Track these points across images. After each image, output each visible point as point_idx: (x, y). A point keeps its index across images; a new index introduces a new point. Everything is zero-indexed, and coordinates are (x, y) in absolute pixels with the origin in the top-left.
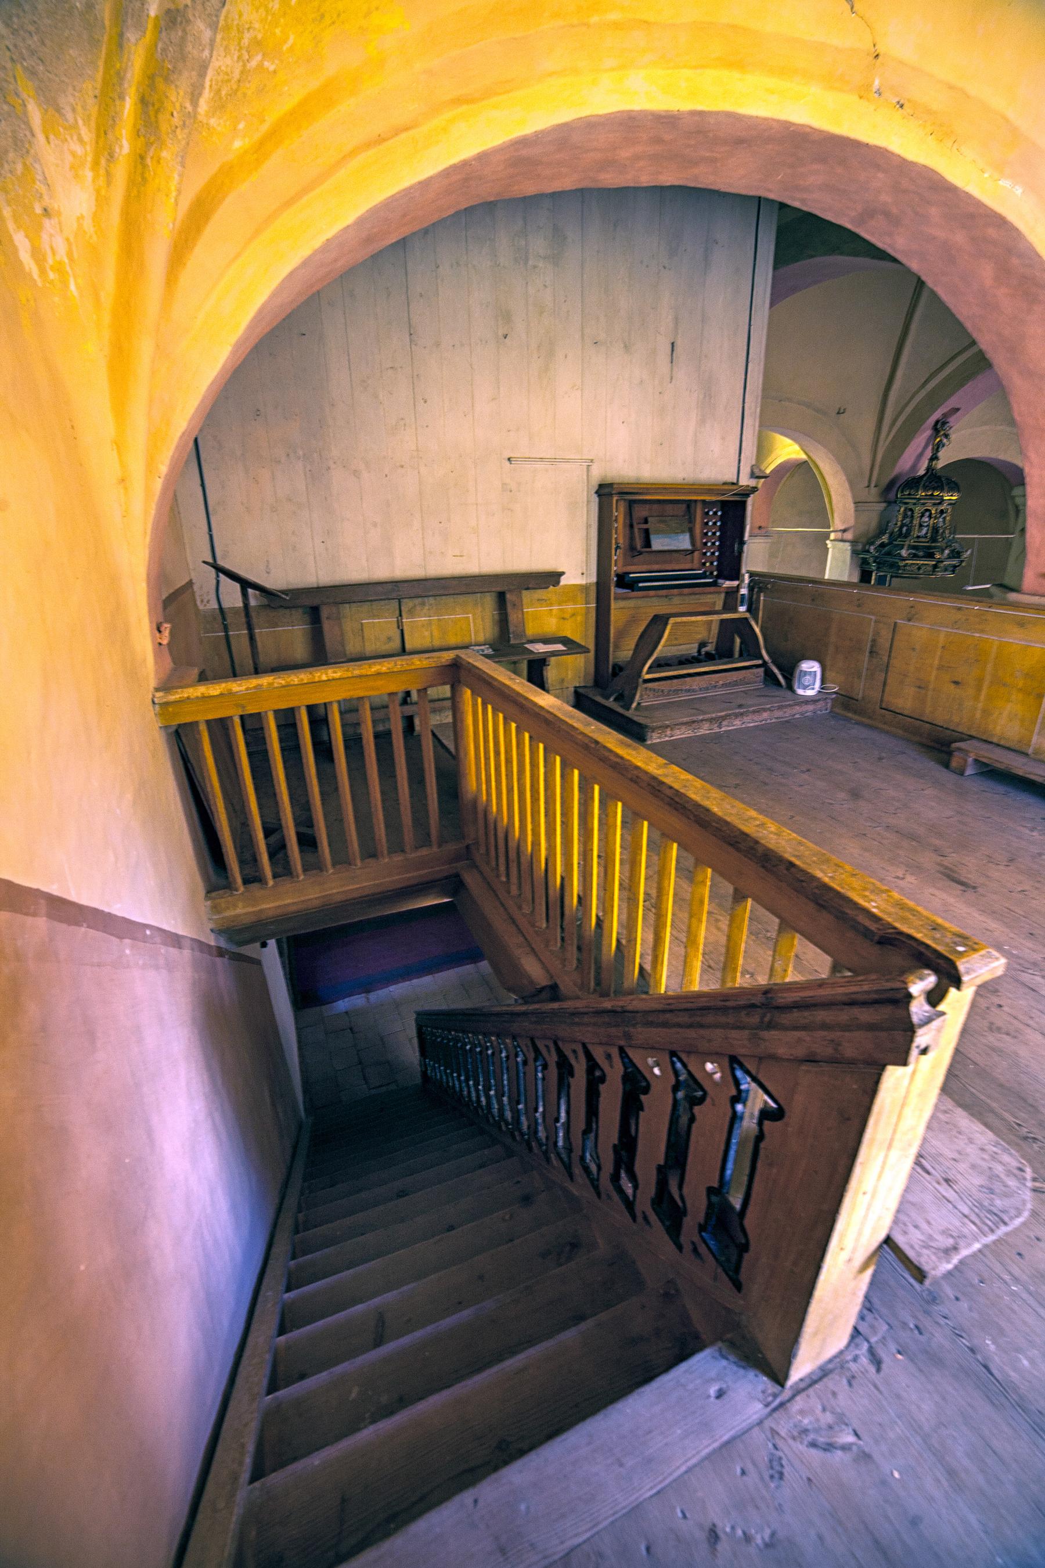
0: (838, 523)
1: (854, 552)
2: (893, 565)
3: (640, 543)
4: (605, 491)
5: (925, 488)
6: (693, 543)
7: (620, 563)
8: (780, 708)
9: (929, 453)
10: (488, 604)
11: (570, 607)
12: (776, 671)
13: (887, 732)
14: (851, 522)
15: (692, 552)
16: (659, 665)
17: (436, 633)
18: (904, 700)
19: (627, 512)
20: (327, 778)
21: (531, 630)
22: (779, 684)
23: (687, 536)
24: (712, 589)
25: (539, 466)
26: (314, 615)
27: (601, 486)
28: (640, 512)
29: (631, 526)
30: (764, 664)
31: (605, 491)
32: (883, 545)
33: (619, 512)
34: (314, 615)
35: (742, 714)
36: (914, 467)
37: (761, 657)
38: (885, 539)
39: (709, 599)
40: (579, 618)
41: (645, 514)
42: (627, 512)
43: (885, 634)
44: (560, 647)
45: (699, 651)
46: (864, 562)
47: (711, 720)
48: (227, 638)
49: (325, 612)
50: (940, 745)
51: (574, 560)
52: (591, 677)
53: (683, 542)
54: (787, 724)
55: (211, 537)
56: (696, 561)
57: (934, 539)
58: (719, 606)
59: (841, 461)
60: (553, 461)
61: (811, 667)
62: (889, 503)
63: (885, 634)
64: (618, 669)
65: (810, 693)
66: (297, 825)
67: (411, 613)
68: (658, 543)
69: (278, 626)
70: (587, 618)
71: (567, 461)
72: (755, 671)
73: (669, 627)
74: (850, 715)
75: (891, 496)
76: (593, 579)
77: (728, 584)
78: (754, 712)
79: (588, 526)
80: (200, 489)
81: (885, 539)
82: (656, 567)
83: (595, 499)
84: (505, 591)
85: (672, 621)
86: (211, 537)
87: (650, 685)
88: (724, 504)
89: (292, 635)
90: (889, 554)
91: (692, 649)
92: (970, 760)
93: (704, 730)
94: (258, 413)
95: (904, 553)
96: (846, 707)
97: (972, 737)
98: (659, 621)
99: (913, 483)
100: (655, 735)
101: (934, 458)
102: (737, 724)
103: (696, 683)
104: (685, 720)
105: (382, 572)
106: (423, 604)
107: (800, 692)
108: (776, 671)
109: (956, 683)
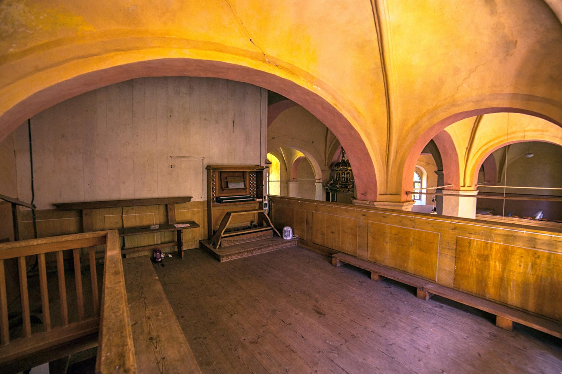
0: (317, 177)
1: (323, 186)
2: (336, 190)
3: (224, 187)
4: (209, 168)
5: (342, 166)
6: (245, 185)
7: (217, 193)
8: (276, 245)
9: (342, 155)
10: (162, 209)
11: (196, 210)
12: (276, 231)
13: (315, 252)
14: (321, 177)
15: (245, 189)
16: (226, 232)
17: (138, 220)
18: (318, 240)
19: (219, 176)
20: (71, 286)
21: (179, 218)
22: (278, 236)
23: (243, 183)
24: (253, 202)
25: (183, 159)
26: (80, 214)
27: (208, 166)
28: (224, 175)
29: (221, 180)
30: (272, 229)
31: (209, 168)
32: (331, 184)
33: (217, 175)
34: (80, 214)
35: (261, 248)
36: (338, 159)
37: (270, 226)
38: (332, 182)
39: (252, 205)
40: (200, 214)
41: (226, 176)
42: (219, 176)
43: (310, 216)
44: (188, 225)
45: (251, 225)
46: (327, 189)
47: (248, 251)
48: (34, 224)
49: (84, 212)
50: (329, 255)
51: (197, 191)
52: (207, 236)
53: (241, 185)
54: (279, 251)
55: (32, 181)
56: (248, 193)
57: (347, 182)
58: (257, 207)
59: (316, 158)
60: (188, 157)
61: (288, 229)
62: (332, 170)
63: (310, 216)
64: (214, 232)
65: (288, 238)
66: (31, 312)
67: (127, 213)
68: (231, 186)
69: (62, 218)
70: (204, 214)
71: (194, 157)
72: (269, 231)
73: (231, 217)
74: (303, 246)
75: (332, 168)
76: (206, 199)
77: (258, 200)
78: (266, 247)
79: (203, 180)
80: (30, 162)
81: (332, 182)
82: (232, 194)
83: (206, 171)
84: (168, 204)
85: (232, 214)
86: (32, 181)
87: (225, 239)
88: (257, 173)
89: (71, 221)
90: (334, 186)
91: (249, 224)
92: (338, 261)
93: (245, 255)
94: (63, 136)
95: (338, 186)
96: (302, 243)
97: (340, 252)
98: (228, 214)
99: (338, 164)
100: (224, 259)
101: (343, 157)
102: (259, 252)
103: (245, 237)
104: (237, 252)
105: (115, 196)
106: (133, 209)
107: (285, 238)
108: (276, 231)
109: (332, 232)
